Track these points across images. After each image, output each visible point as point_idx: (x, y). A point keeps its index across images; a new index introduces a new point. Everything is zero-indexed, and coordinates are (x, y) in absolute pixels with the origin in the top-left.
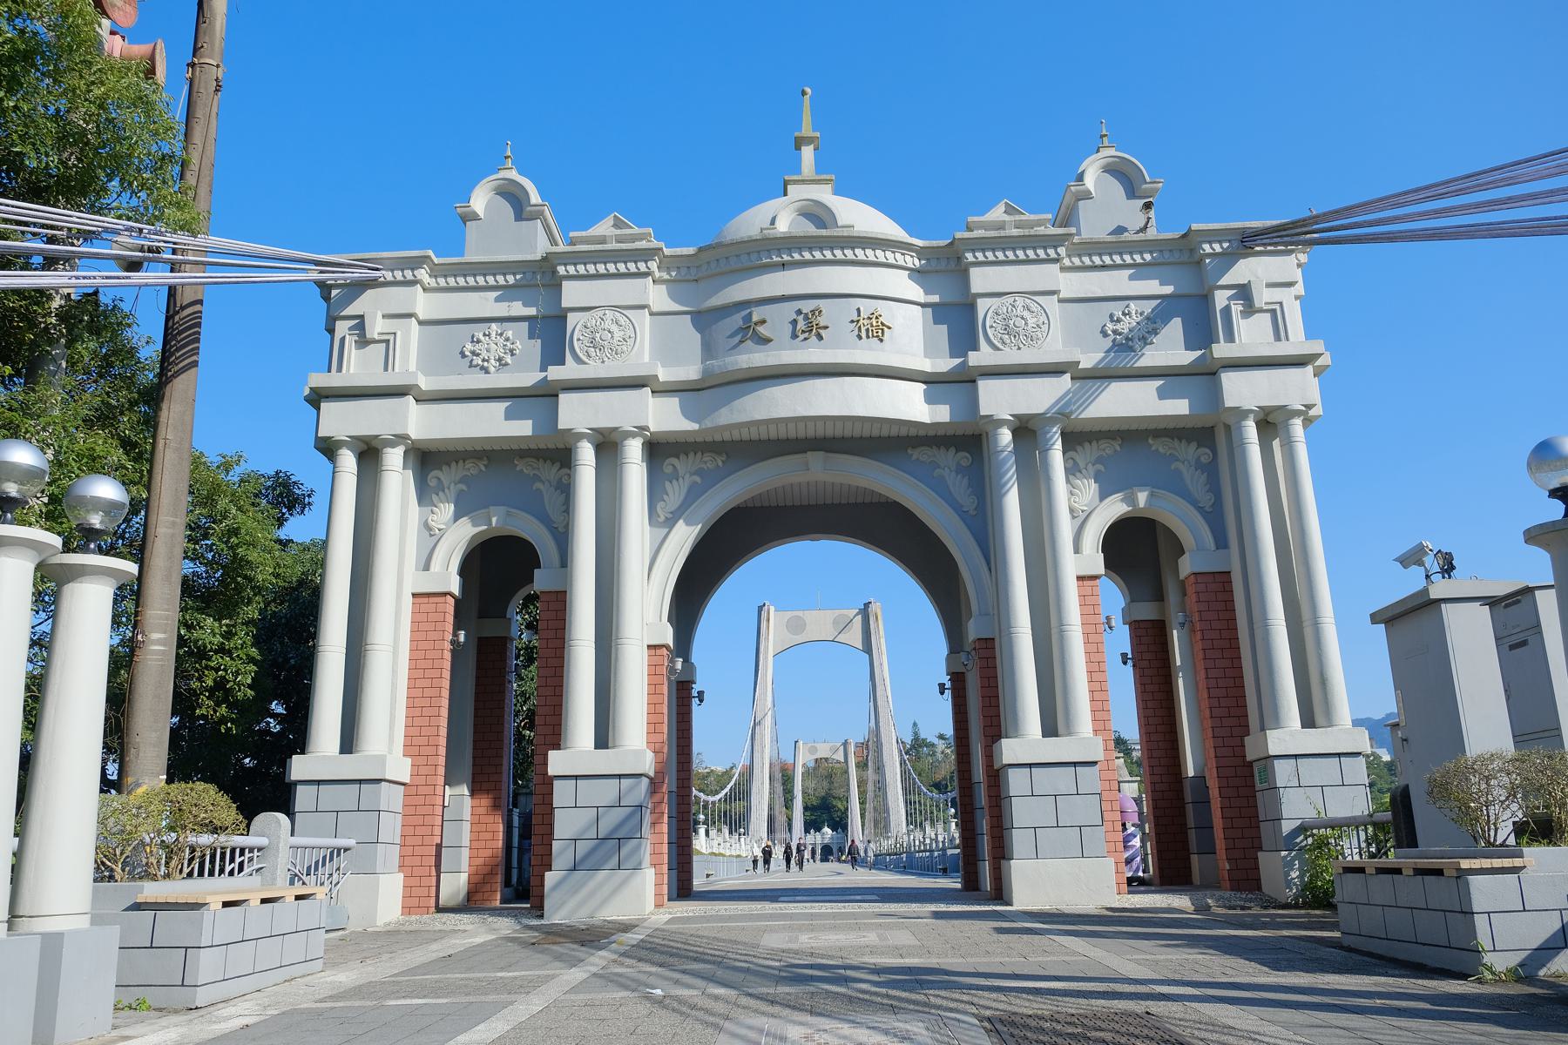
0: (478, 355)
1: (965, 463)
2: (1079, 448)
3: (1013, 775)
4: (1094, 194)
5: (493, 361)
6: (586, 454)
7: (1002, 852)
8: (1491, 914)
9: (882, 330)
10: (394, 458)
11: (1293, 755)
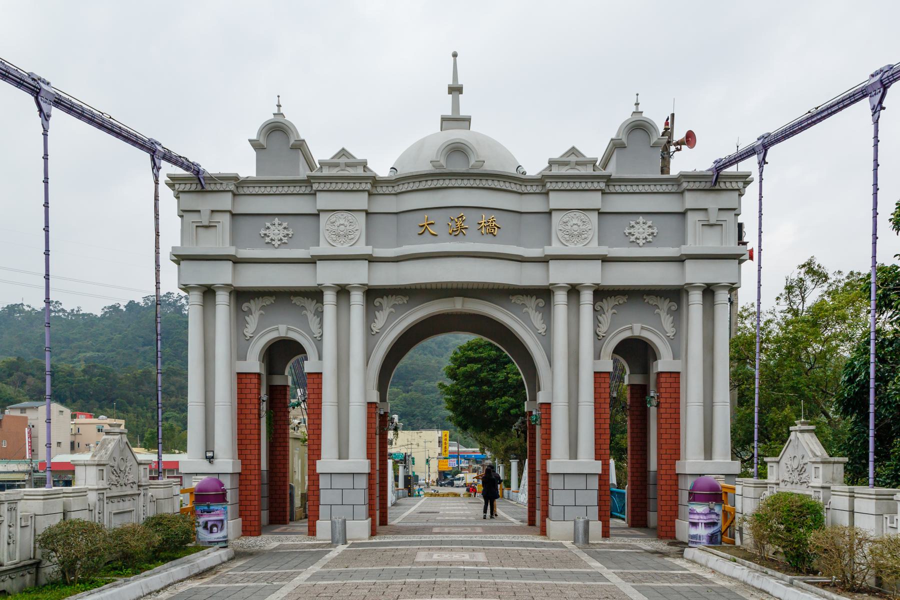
1: (541, 305)
2: (252, 301)
3: (321, 478)
7: (546, 515)
9: (494, 229)
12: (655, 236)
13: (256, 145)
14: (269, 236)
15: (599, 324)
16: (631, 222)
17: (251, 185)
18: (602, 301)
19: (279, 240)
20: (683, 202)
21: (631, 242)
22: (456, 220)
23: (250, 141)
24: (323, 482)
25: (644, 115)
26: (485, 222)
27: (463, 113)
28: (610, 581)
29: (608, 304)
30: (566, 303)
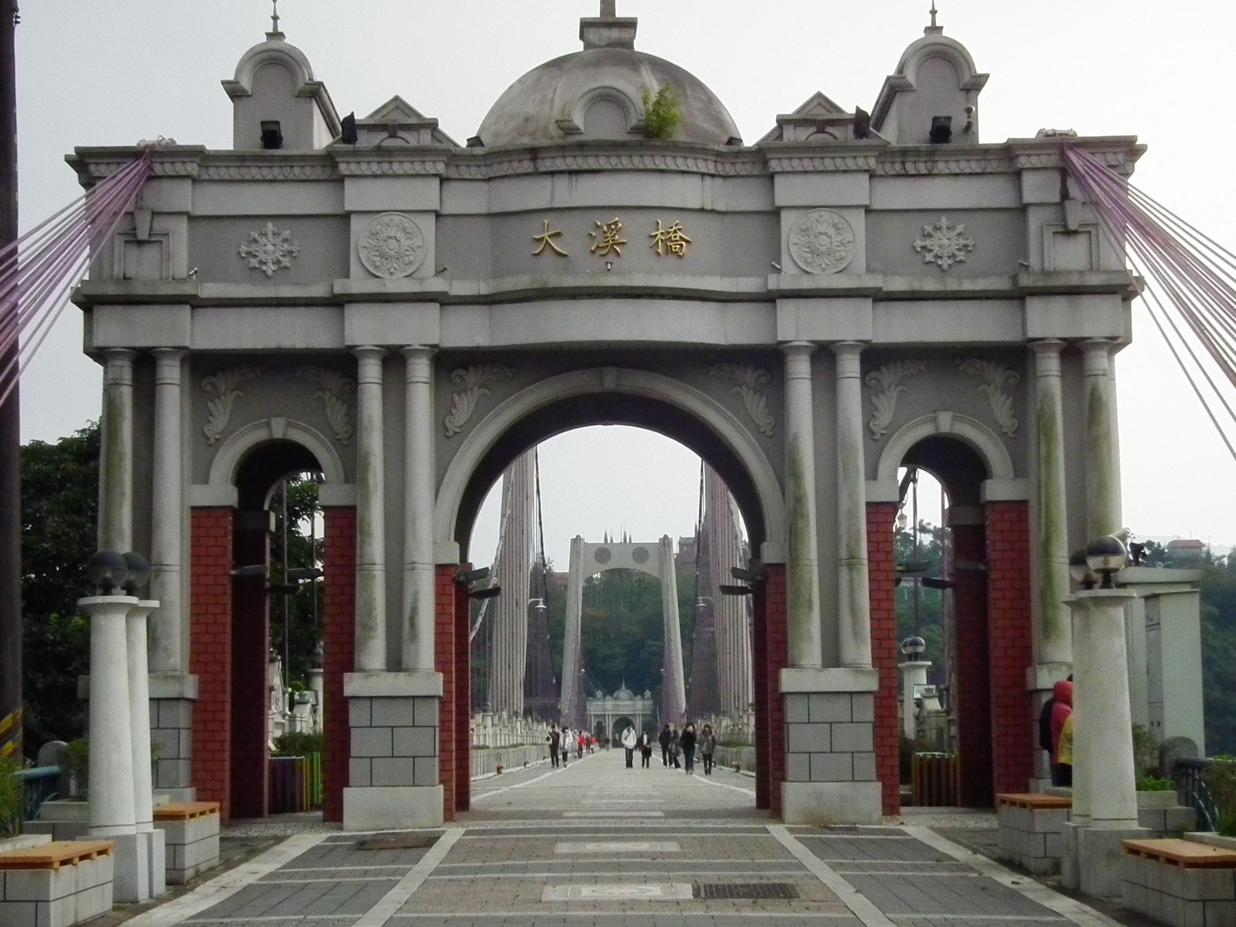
0: (255, 256)
4: (582, 129)
5: (270, 265)
6: (371, 371)
8: (1047, 835)
10: (171, 373)
11: (804, 693)
12: (295, 257)
13: (234, 91)
14: (931, 251)
15: (211, 418)
16: (252, 233)
17: (1034, 152)
18: (880, 371)
19: (949, 257)
20: (341, 198)
21: (927, 263)
22: (605, 228)
23: (223, 83)
24: (356, 715)
25: (945, 33)
26: (662, 233)
27: (938, 24)
28: (841, 875)
29: (887, 376)
30: (381, 382)
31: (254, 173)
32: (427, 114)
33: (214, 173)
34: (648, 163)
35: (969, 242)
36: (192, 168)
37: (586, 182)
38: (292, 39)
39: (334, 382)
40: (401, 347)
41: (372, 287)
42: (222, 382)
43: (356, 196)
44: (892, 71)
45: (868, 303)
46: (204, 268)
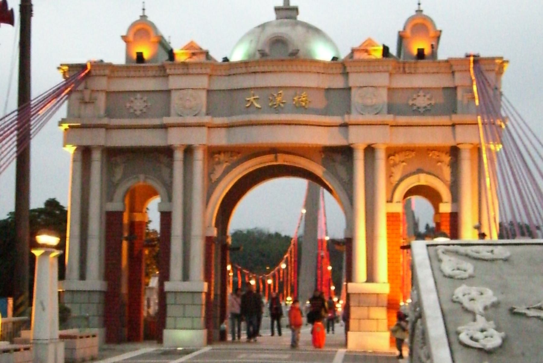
6: (179, 155)
24: (170, 299)
31: (132, 74)
32: (205, 47)
33: (116, 74)
34: (295, 68)
35: (149, 104)
36: (107, 72)
37: (259, 77)
38: (151, 18)
39: (165, 159)
40: (191, 145)
41: (179, 120)
42: (119, 159)
43: (174, 82)
44: (401, 29)
45: (104, 130)
46: (109, 114)
